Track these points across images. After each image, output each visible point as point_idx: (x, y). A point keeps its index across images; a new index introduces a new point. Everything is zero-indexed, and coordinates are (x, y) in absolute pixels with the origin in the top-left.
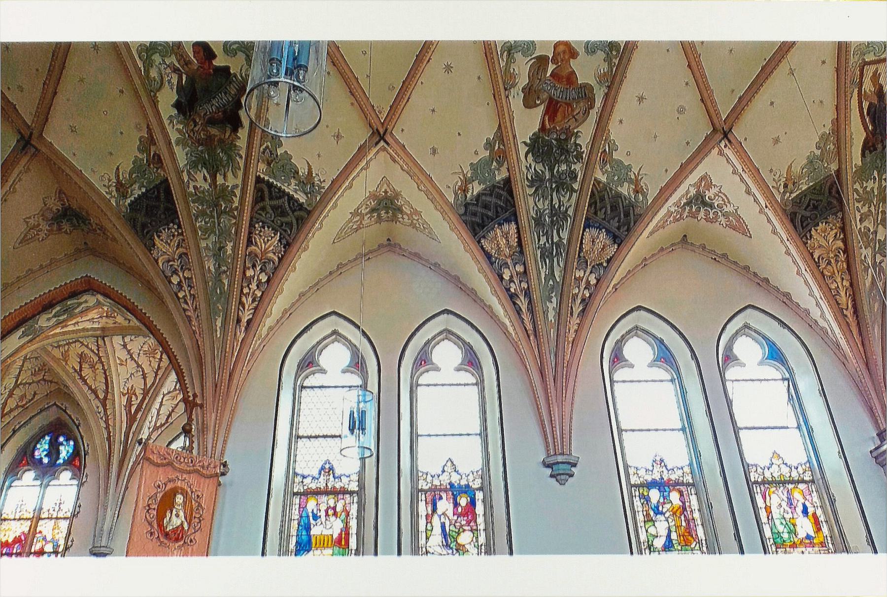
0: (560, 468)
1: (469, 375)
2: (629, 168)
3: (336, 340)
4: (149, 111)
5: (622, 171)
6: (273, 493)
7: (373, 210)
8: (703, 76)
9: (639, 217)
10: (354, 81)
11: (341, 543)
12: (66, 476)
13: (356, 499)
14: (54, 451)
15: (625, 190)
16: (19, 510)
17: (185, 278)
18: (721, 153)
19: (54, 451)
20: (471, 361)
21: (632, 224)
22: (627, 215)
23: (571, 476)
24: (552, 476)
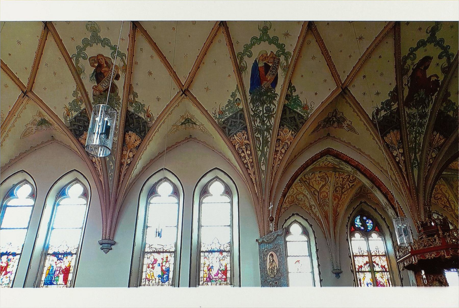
0: (108, 244)
1: (227, 198)
2: (143, 106)
3: (216, 180)
4: (8, 71)
5: (140, 107)
6: (33, 257)
7: (182, 124)
8: (35, 62)
9: (149, 128)
10: (356, 69)
11: (164, 277)
12: (374, 236)
13: (173, 255)
14: (364, 224)
15: (142, 115)
16: (360, 251)
17: (244, 153)
18: (347, 102)
19: (364, 224)
20: (228, 192)
21: (147, 131)
22: (144, 126)
23: (111, 249)
24: (102, 249)
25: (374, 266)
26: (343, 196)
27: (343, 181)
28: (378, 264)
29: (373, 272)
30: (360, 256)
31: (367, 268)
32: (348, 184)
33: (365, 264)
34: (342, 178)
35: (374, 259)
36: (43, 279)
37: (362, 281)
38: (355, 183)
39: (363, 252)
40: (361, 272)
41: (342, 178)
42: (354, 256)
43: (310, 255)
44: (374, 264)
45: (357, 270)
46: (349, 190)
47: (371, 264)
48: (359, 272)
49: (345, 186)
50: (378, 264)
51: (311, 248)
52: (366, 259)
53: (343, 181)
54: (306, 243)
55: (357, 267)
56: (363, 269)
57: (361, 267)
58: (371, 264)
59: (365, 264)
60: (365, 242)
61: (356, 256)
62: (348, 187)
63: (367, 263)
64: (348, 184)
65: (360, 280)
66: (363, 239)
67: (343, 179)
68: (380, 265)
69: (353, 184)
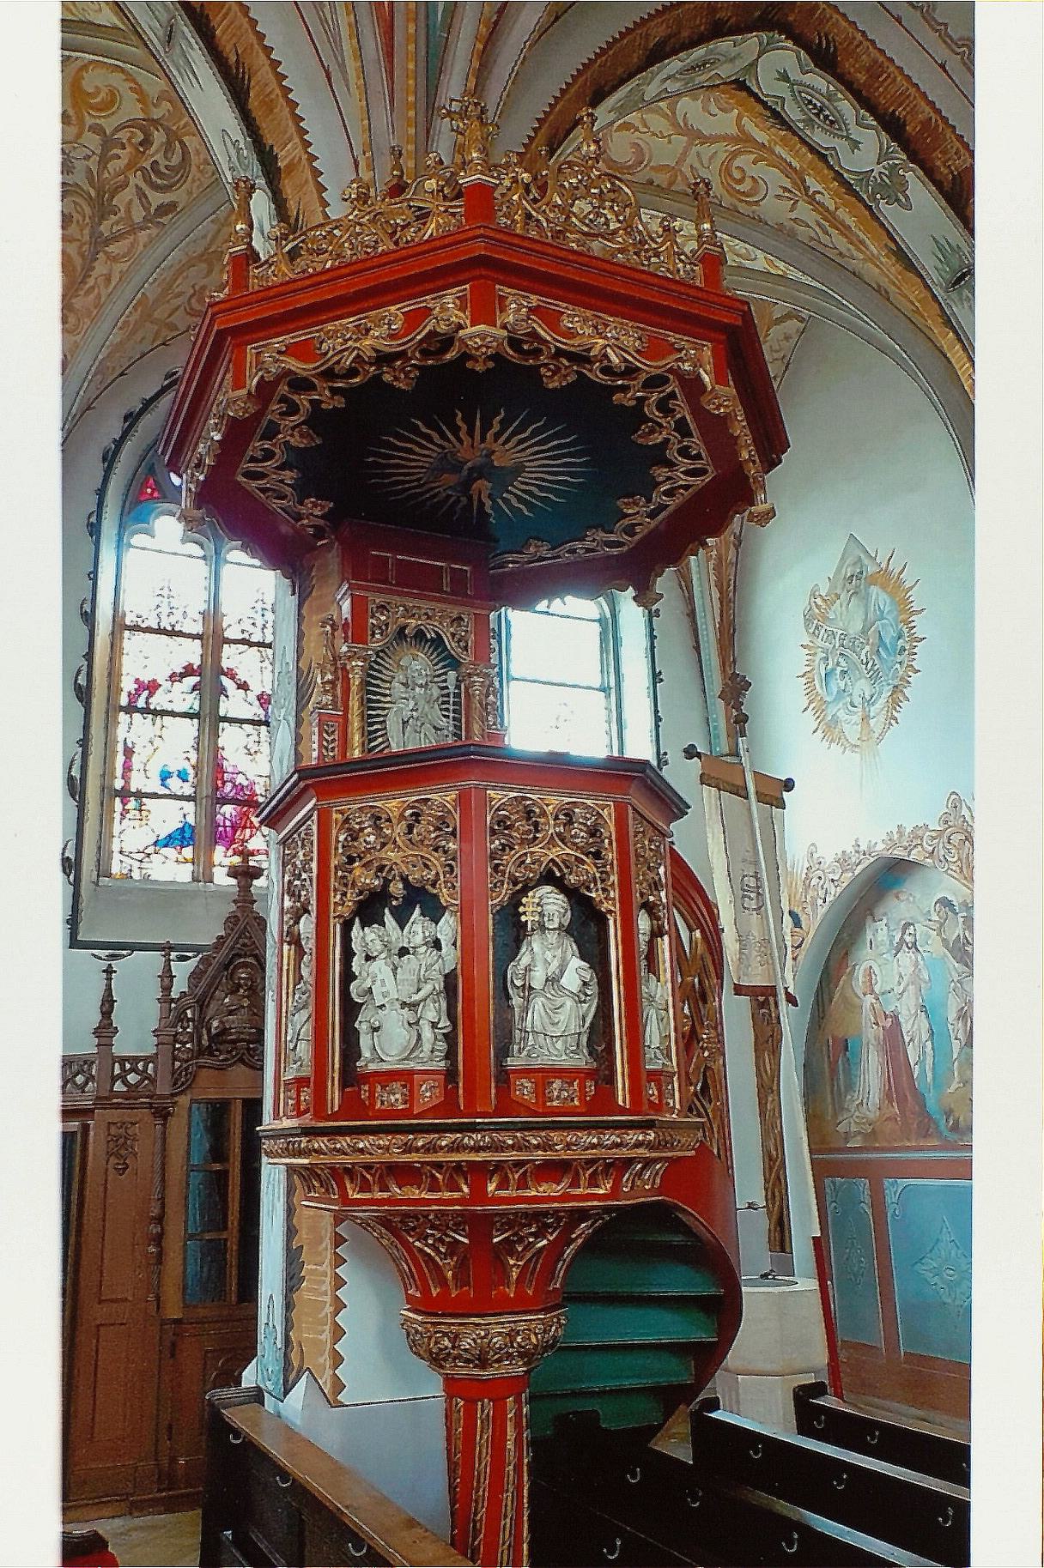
16: (165, 610)
25: (223, 691)
26: (100, 268)
27: (104, 161)
28: (243, 686)
29: (209, 719)
30: (160, 631)
31: (181, 697)
32: (141, 195)
33: (174, 678)
34: (97, 129)
35: (231, 657)
36: (789, 944)
37: (136, 761)
38: (178, 195)
39: (178, 615)
40: (146, 711)
41: (97, 129)
42: (120, 626)
43: (613, 689)
44: (225, 681)
45: (124, 701)
46: (143, 236)
47: (209, 678)
48: (131, 709)
49: (119, 201)
50: (243, 686)
51: (623, 652)
52: (192, 652)
53: (104, 161)
54: (596, 627)
55: (128, 685)
56: (159, 701)
57: (153, 687)
58: (209, 678)
59: (174, 678)
60: (202, 569)
61: (136, 628)
62: (138, 214)
63: (189, 671)
64: (141, 195)
65: (129, 752)
66: (196, 550)
67: (108, 143)
68: (256, 689)
69: (167, 198)
